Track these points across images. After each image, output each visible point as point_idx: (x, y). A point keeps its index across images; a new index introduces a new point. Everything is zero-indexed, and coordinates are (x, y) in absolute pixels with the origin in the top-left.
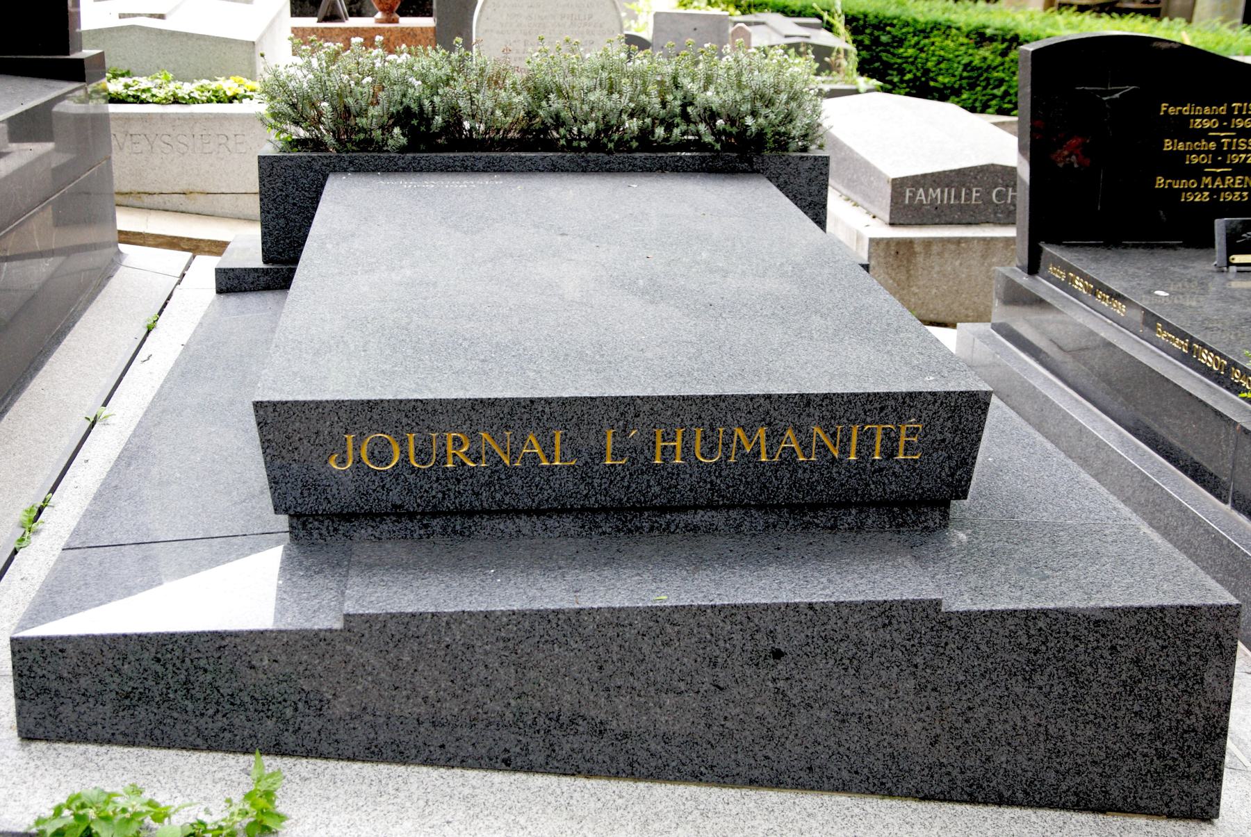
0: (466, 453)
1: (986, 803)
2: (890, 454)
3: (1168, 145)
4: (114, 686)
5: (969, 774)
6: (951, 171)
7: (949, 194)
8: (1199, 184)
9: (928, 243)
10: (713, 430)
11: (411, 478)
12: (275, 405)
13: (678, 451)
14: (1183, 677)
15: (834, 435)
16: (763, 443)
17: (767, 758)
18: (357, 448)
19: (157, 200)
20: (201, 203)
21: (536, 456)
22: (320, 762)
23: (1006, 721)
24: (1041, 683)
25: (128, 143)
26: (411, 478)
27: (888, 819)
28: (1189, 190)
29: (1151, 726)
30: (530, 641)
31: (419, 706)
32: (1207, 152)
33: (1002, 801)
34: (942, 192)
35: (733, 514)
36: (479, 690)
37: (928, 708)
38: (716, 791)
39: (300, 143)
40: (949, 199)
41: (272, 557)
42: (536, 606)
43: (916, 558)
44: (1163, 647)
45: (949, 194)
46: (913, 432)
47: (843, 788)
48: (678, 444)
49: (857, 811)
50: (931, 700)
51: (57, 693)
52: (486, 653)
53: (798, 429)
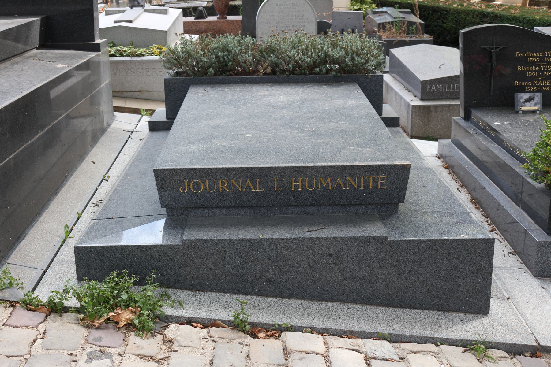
0: (226, 187)
1: (406, 308)
2: (375, 187)
3: (519, 69)
4: (107, 263)
5: (399, 297)
6: (446, 77)
7: (445, 87)
8: (532, 84)
9: (436, 107)
10: (312, 178)
11: (208, 195)
12: (161, 170)
13: (300, 186)
14: (475, 264)
15: (355, 180)
16: (330, 183)
17: (328, 291)
18: (189, 185)
19: (129, 94)
20: (146, 95)
21: (250, 188)
22: (175, 290)
23: (412, 279)
24: (424, 266)
25: (118, 72)
26: (208, 195)
27: (370, 312)
28: (528, 86)
29: (464, 281)
30: (245, 250)
31: (208, 271)
32: (536, 71)
33: (411, 307)
34: (443, 86)
35: (321, 208)
36: (228, 266)
37: (384, 274)
38: (310, 302)
39: (178, 74)
40: (445, 89)
41: (161, 223)
42: (247, 237)
43: (383, 223)
44: (467, 253)
45: (445, 87)
46: (383, 179)
47: (355, 302)
48: (300, 183)
49: (359, 309)
50: (385, 272)
51: (89, 265)
52: (230, 254)
53: (342, 178)
